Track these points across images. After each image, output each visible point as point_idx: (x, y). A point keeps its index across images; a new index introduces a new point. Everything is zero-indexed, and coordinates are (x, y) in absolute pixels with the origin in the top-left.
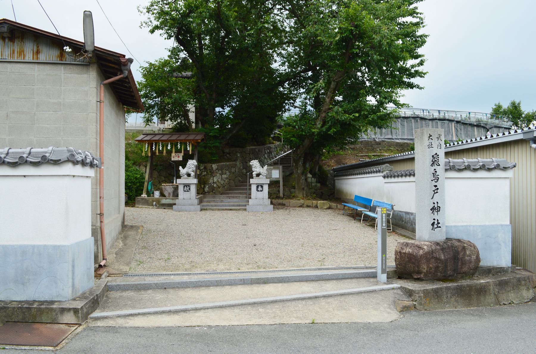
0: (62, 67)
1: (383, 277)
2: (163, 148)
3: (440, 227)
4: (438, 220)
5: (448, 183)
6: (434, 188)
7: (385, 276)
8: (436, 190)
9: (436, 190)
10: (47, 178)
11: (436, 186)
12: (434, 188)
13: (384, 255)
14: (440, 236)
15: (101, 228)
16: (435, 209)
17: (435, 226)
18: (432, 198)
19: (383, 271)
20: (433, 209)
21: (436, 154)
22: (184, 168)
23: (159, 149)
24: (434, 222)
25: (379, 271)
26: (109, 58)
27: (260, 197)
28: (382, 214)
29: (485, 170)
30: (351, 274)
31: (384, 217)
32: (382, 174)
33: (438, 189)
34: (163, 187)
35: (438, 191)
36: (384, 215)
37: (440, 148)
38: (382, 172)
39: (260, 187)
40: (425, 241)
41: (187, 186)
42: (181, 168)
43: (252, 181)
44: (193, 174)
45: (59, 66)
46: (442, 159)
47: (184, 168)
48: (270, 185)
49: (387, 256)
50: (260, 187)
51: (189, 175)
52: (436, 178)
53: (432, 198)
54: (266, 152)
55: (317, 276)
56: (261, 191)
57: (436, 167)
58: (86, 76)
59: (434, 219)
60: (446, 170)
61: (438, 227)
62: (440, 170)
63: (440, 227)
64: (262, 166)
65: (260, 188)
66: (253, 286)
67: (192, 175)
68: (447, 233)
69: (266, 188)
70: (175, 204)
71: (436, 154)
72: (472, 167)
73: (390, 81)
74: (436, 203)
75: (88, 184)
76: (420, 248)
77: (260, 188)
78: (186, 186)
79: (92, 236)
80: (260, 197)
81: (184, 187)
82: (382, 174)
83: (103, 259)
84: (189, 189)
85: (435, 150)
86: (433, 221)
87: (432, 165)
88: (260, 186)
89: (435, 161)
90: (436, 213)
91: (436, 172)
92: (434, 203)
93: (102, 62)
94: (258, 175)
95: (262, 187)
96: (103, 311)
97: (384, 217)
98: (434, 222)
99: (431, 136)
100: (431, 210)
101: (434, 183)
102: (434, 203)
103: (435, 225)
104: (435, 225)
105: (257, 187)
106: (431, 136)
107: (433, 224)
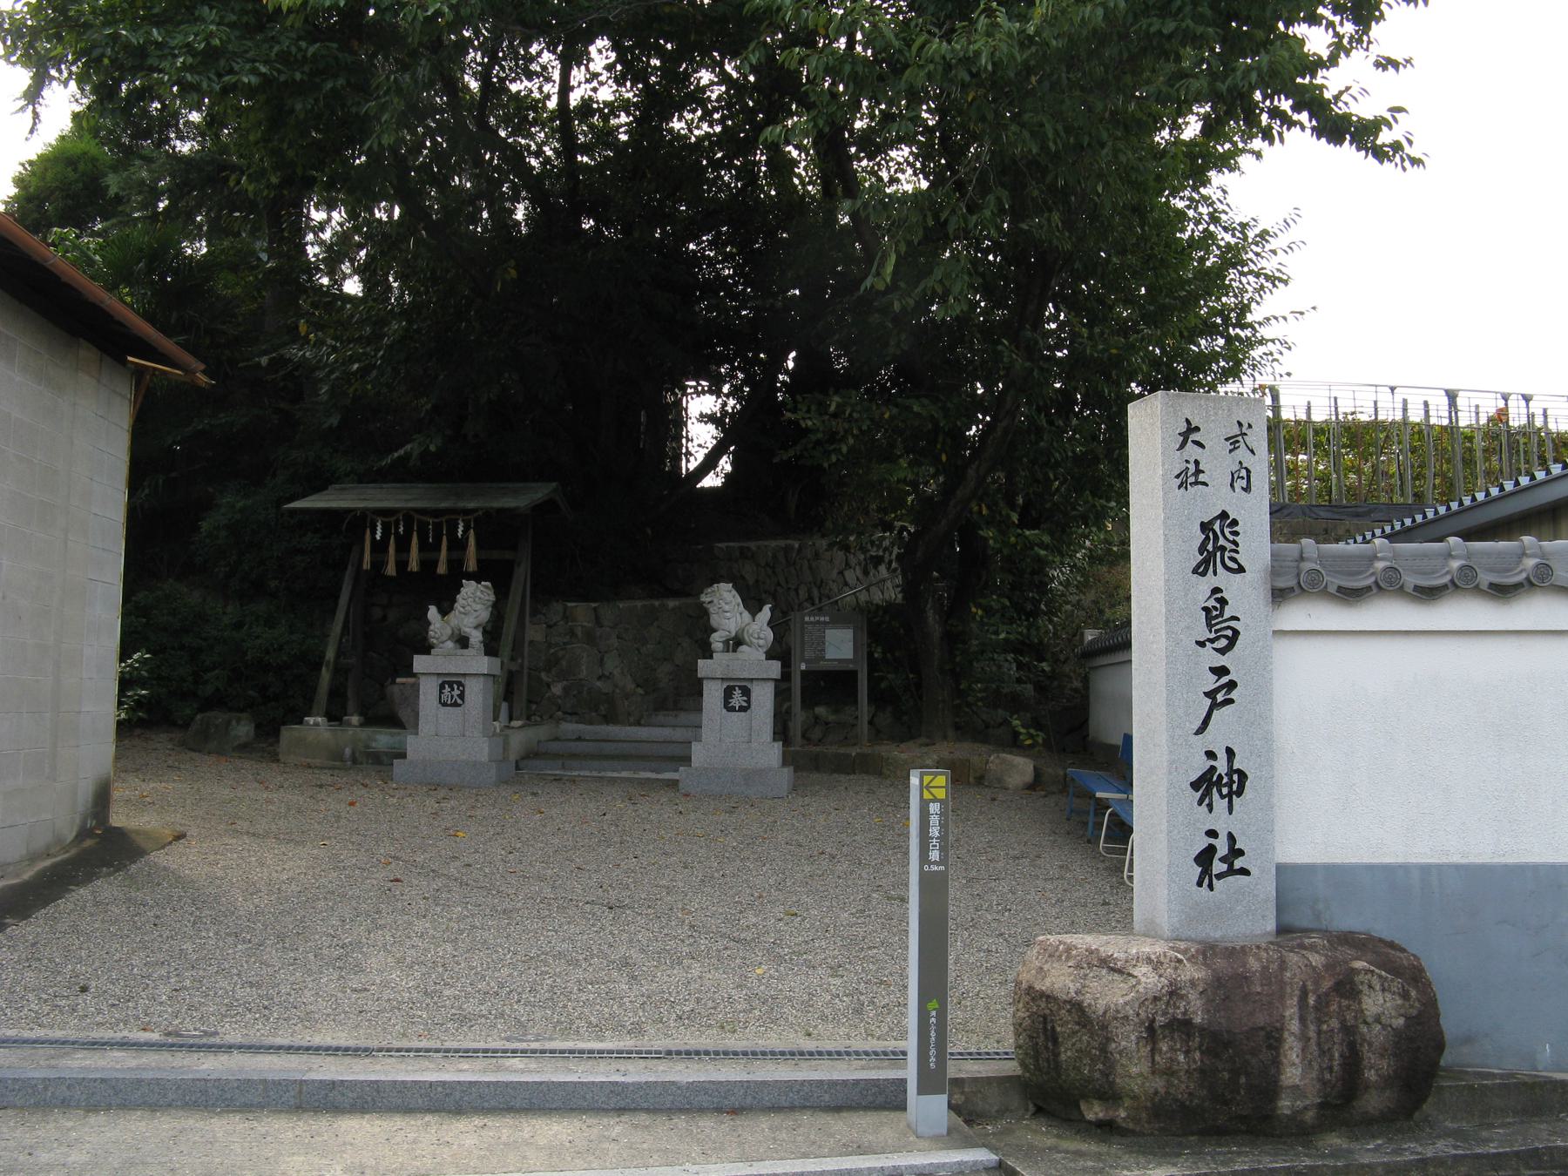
1: (931, 1110)
3: (1244, 872)
6: (1211, 682)
7: (939, 1102)
9: (1223, 691)
11: (1220, 671)
12: (1211, 682)
13: (933, 1005)
14: (1245, 912)
17: (1218, 867)
19: (929, 1083)
20: (1206, 784)
22: (444, 612)
24: (1211, 850)
25: (910, 1073)
27: (736, 734)
29: (1477, 591)
30: (790, 1085)
31: (934, 820)
33: (1232, 685)
34: (396, 689)
35: (1234, 695)
36: (934, 808)
37: (1247, 489)
39: (737, 692)
41: (452, 685)
42: (433, 612)
44: (476, 637)
50: (737, 692)
51: (463, 642)
52: (1220, 626)
55: (615, 1088)
56: (743, 709)
57: (1222, 578)
59: (1212, 833)
60: (1279, 596)
61: (1231, 871)
62: (1245, 595)
63: (1244, 872)
64: (753, 606)
65: (738, 699)
66: (93, 1119)
67: (472, 641)
71: (1224, 515)
72: (1410, 580)
78: (451, 684)
80: (736, 734)
81: (442, 687)
84: (462, 696)
85: (1216, 497)
86: (1205, 842)
87: (1201, 570)
89: (1215, 545)
90: (1220, 804)
91: (1223, 602)
92: (1211, 755)
94: (736, 643)
95: (746, 692)
96: (959, 1163)
97: (934, 820)
98: (1211, 850)
99: (1191, 429)
100: (1195, 785)
101: (1210, 657)
102: (1211, 755)
103: (1215, 861)
105: (728, 693)
107: (1205, 858)
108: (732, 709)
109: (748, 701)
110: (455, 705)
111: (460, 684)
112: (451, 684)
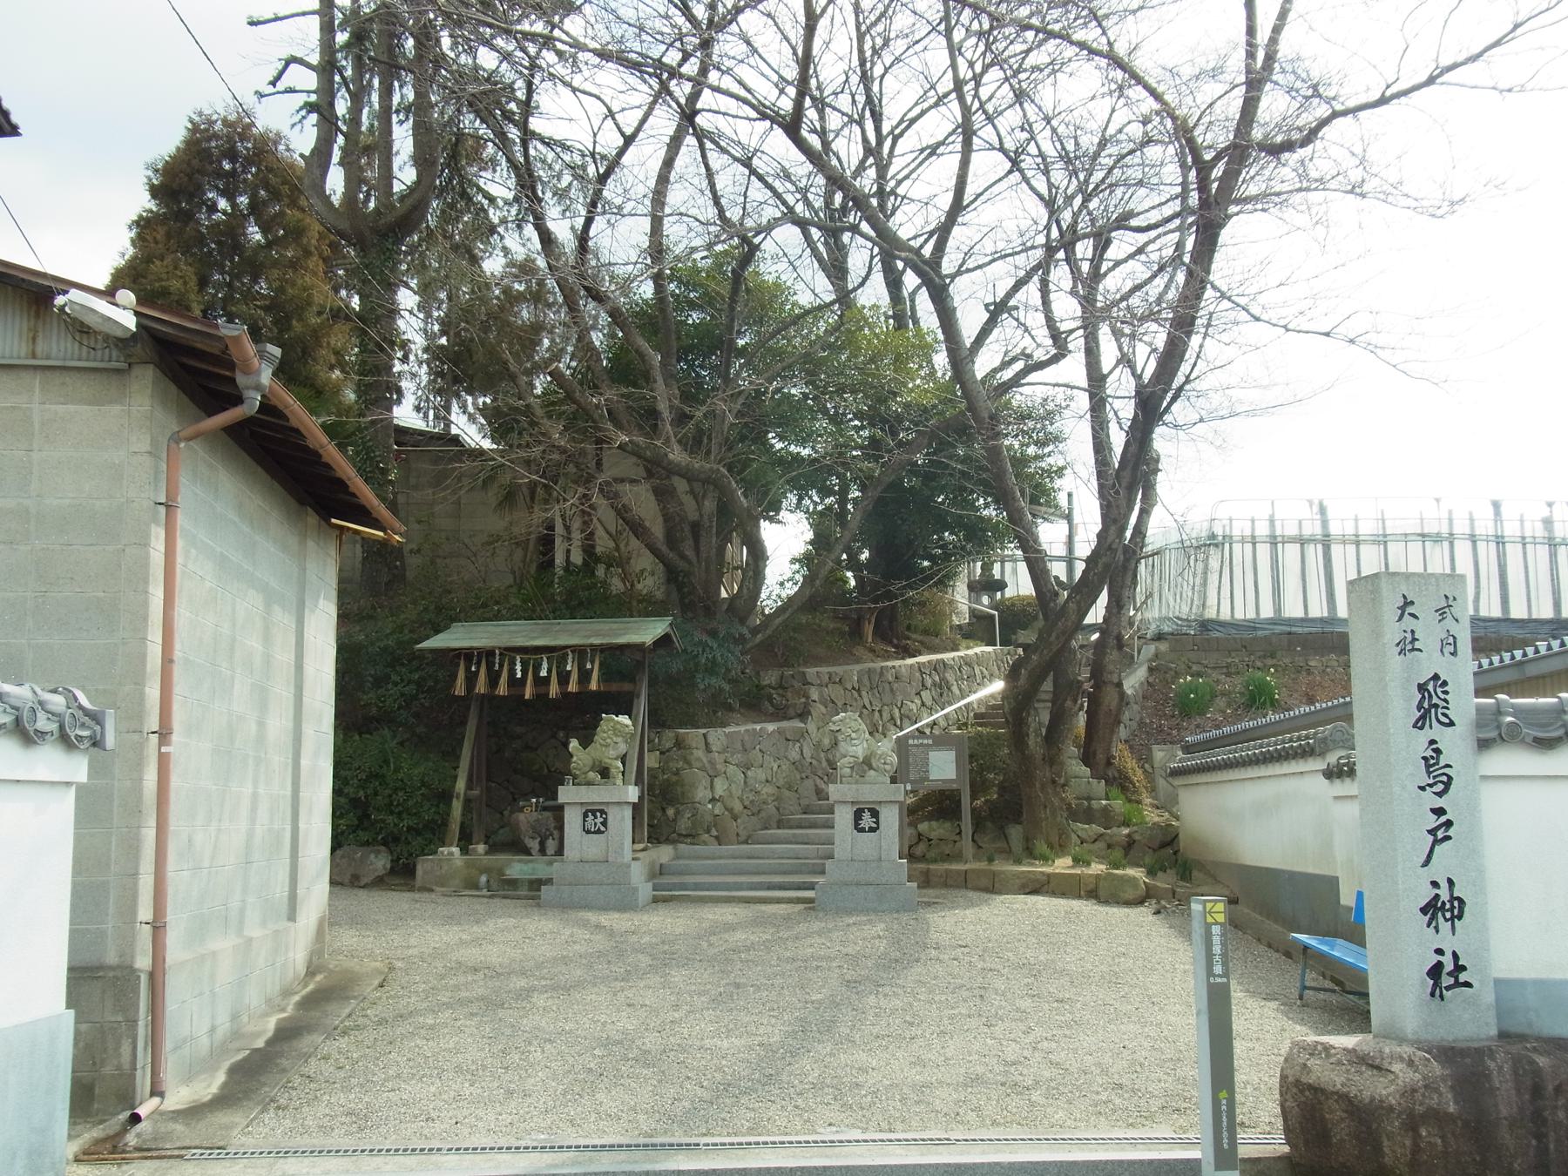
0: (37, 380)
2: (525, 672)
3: (1468, 984)
4: (1455, 956)
5: (1488, 793)
6: (1432, 821)
8: (1442, 830)
9: (1442, 830)
10: (19, 786)
11: (1439, 812)
12: (1432, 821)
13: (1223, 1094)
14: (1470, 1019)
15: (152, 975)
16: (1443, 908)
17: (1447, 981)
18: (1427, 863)
20: (1432, 909)
21: (1436, 677)
22: (586, 742)
23: (512, 672)
24: (1439, 965)
26: (199, 346)
28: (1208, 927)
32: (1320, 765)
33: (1449, 824)
36: (1216, 930)
37: (1454, 654)
38: (1322, 754)
39: (867, 815)
40: (1401, 1040)
42: (574, 744)
43: (834, 791)
45: (26, 377)
46: (1464, 702)
47: (586, 742)
48: (913, 813)
49: (1239, 1098)
50: (867, 815)
53: (1427, 863)
54: (929, 682)
56: (872, 830)
57: (1436, 731)
58: (116, 409)
59: (1439, 952)
60: (1484, 745)
61: (1457, 984)
62: (1455, 744)
63: (1468, 984)
65: (867, 820)
68: (1501, 1010)
69: (891, 819)
70: (549, 881)
71: (1436, 677)
73: (785, 374)
74: (1444, 885)
75: (67, 803)
76: (1379, 1068)
77: (867, 820)
78: (594, 812)
79: (68, 1007)
81: (585, 815)
82: (1320, 765)
83: (153, 1094)
84: (604, 824)
85: (1430, 662)
87: (1419, 724)
88: (865, 816)
89: (1430, 704)
90: (1445, 927)
91: (1438, 751)
92: (1435, 884)
93: (185, 360)
95: (875, 814)
98: (1439, 965)
100: (1424, 910)
102: (1435, 884)
103: (1445, 976)
104: (1445, 976)
105: (858, 815)
106: (1407, 603)
107: (1435, 971)
108: (862, 830)
109: (877, 823)
110: (599, 832)
111: (602, 812)
112: (594, 812)
